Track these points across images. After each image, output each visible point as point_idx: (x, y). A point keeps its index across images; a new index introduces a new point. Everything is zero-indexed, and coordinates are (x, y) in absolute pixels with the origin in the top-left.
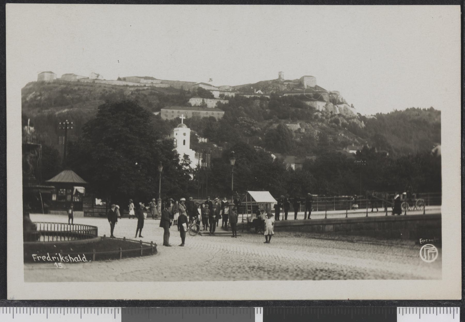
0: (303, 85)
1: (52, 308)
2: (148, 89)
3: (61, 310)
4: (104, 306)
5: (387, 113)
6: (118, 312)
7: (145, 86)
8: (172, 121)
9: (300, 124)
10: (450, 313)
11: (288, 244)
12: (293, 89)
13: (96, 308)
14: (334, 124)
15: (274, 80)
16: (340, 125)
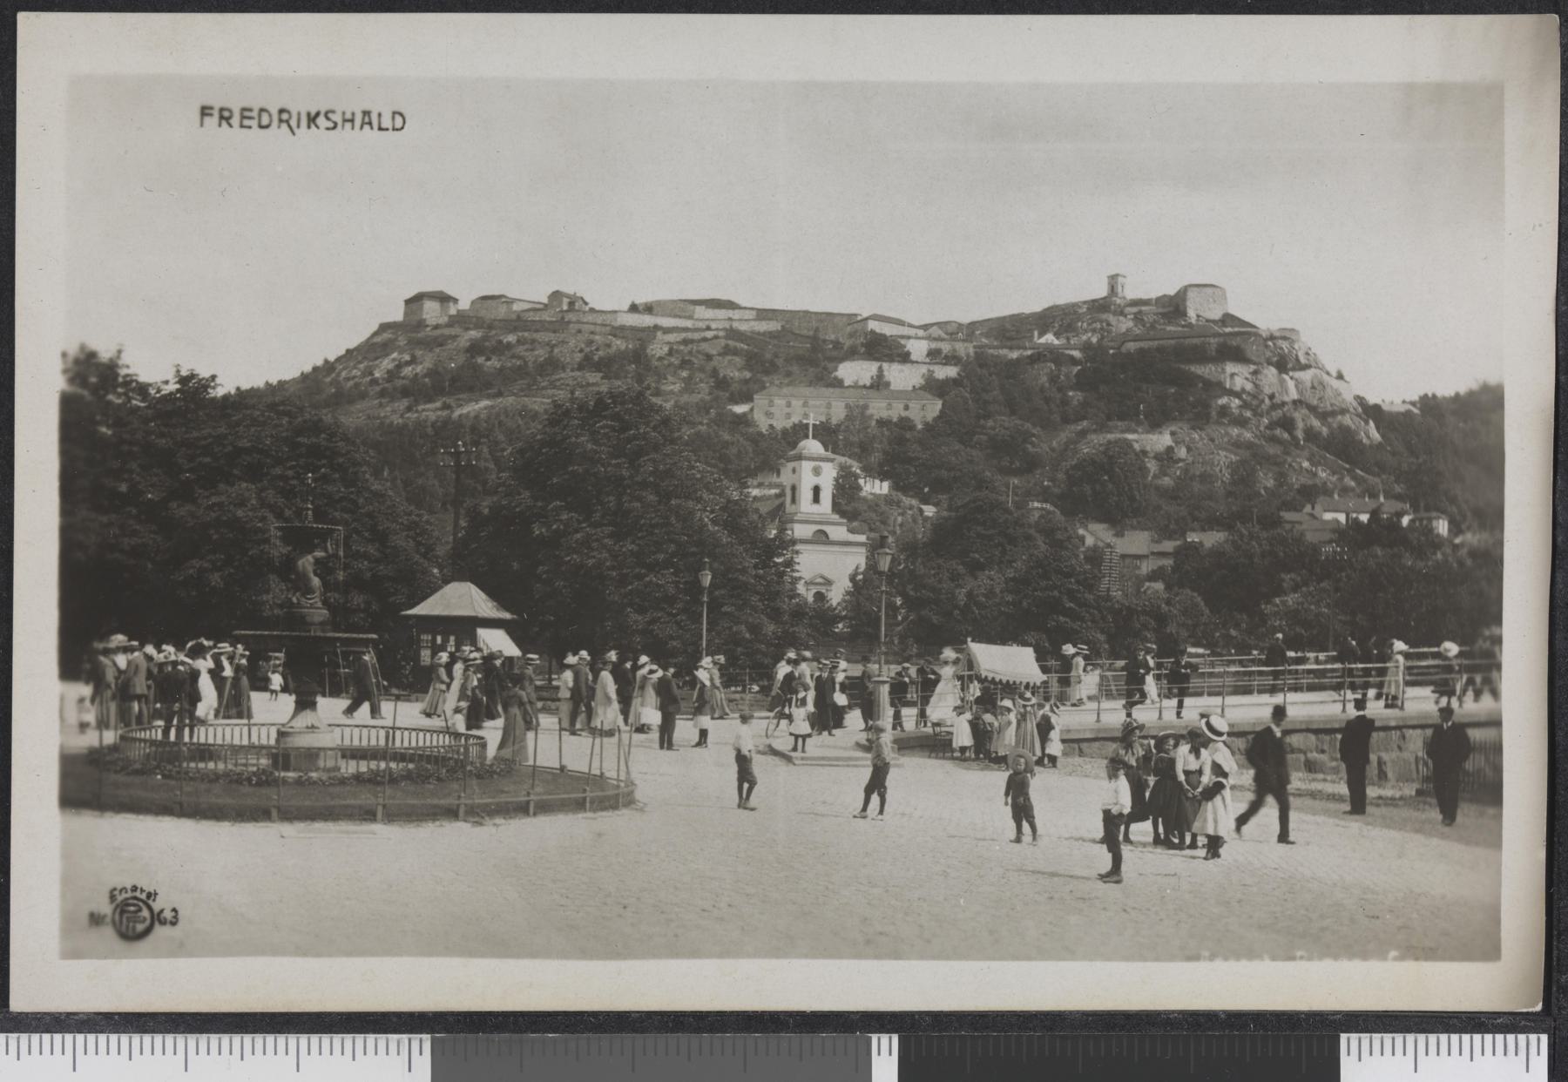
0: (1184, 314)
1: (203, 1038)
2: (716, 337)
3: (231, 1045)
4: (374, 1032)
5: (1453, 394)
6: (421, 1048)
7: (708, 328)
8: (785, 432)
9: (1173, 434)
10: (1516, 1054)
11: (348, 832)
12: (1153, 327)
13: (348, 1038)
14: (1278, 432)
15: (1094, 301)
16: (1300, 434)
